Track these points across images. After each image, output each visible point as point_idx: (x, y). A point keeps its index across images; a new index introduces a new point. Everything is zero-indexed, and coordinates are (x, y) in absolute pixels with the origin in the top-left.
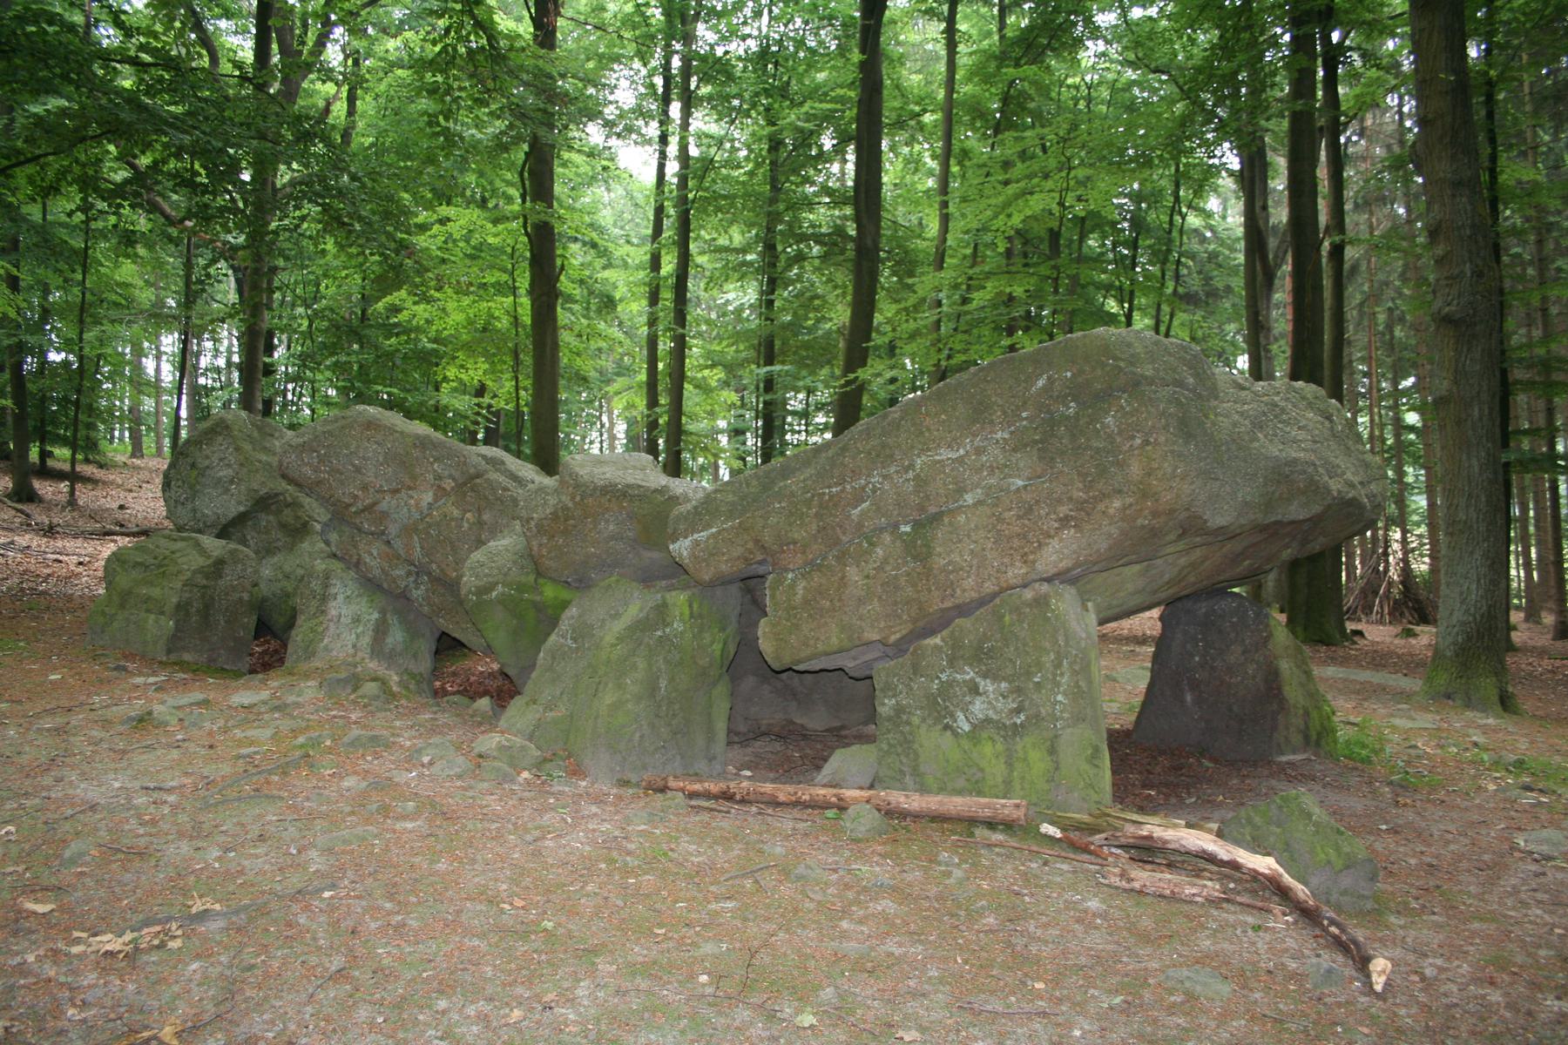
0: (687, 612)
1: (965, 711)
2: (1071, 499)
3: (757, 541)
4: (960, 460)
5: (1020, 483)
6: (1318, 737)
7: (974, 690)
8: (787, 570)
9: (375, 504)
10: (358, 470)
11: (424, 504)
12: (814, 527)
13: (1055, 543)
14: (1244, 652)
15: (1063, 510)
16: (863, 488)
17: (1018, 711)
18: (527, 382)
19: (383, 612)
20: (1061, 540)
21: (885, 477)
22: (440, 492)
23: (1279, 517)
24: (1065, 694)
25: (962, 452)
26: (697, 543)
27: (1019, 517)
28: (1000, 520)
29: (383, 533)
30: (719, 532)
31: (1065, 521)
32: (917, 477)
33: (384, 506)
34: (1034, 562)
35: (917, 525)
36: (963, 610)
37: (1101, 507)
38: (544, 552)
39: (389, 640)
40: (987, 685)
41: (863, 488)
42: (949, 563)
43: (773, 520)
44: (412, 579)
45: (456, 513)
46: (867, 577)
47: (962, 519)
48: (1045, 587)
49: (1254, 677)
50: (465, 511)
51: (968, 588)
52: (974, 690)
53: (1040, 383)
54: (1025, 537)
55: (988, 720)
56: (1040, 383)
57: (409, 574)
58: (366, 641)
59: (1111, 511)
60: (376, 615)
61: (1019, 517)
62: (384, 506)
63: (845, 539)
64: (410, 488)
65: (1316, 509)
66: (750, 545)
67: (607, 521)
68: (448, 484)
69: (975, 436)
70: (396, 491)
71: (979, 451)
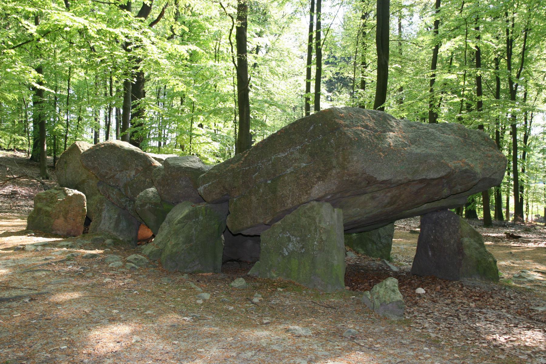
0: (204, 212)
1: (286, 248)
2: (320, 170)
3: (224, 187)
4: (286, 157)
5: (304, 165)
6: (489, 271)
7: (289, 240)
8: (234, 197)
9: (114, 175)
10: (108, 163)
11: (132, 176)
12: (241, 181)
13: (316, 186)
14: (450, 234)
15: (318, 174)
16: (256, 167)
17: (302, 248)
18: (238, 127)
19: (119, 215)
20: (318, 185)
21: (262, 163)
22: (137, 171)
23: (424, 177)
24: (317, 242)
25: (286, 154)
26: (205, 188)
27: (304, 177)
28: (298, 178)
29: (118, 186)
30: (212, 184)
31: (319, 179)
32: (272, 163)
33: (117, 176)
34: (310, 194)
35: (273, 181)
36: (289, 211)
37: (329, 173)
38: (162, 192)
39: (121, 225)
40: (293, 239)
41: (256, 167)
42: (282, 194)
43: (228, 179)
44: (128, 203)
45: (143, 179)
46: (258, 200)
47: (286, 178)
48: (315, 203)
49: (453, 245)
50: (146, 178)
51: (289, 203)
52: (289, 240)
53: (311, 128)
54: (307, 184)
55: (293, 251)
56: (311, 128)
57: (126, 201)
58: (112, 225)
59: (333, 174)
60: (116, 216)
61: (304, 177)
62: (117, 176)
63: (251, 186)
64: (126, 170)
65: (443, 174)
66: (222, 189)
67: (182, 181)
68: (140, 168)
69: (290, 148)
70: (121, 171)
71: (292, 153)
